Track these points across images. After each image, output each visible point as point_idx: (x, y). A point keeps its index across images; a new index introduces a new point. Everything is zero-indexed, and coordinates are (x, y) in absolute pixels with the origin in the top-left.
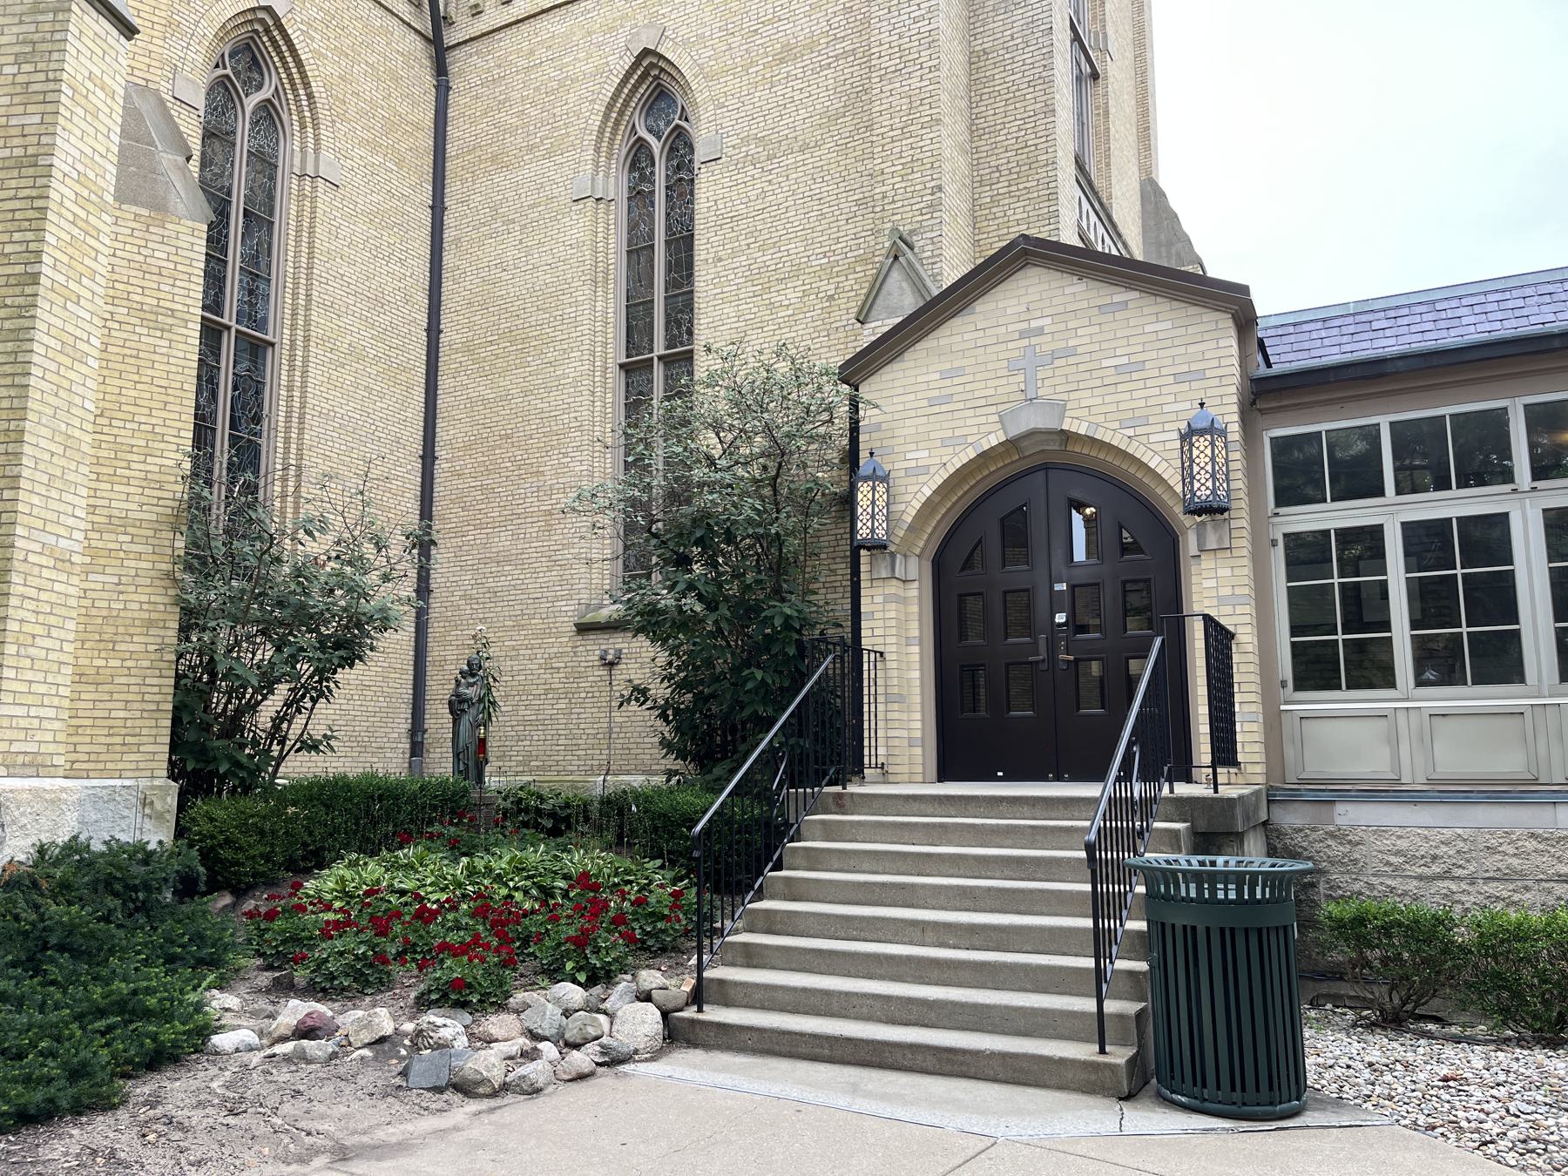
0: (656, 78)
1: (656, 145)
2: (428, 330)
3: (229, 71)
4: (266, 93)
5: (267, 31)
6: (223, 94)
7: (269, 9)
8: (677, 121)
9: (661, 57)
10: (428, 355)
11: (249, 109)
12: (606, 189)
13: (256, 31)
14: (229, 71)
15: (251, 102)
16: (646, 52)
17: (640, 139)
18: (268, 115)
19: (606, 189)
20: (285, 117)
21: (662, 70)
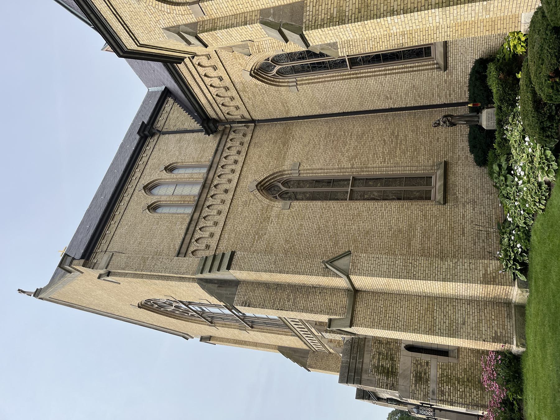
0: (257, 70)
1: (278, 68)
2: (344, 112)
3: (277, 195)
4: (280, 185)
5: (262, 186)
6: (283, 196)
7: (257, 186)
8: (270, 62)
9: (251, 70)
10: (351, 112)
11: (286, 189)
12: (297, 173)
13: (264, 188)
14: (277, 195)
15: (284, 189)
16: (251, 75)
17: (276, 73)
18: (286, 183)
19: (297, 173)
20: (285, 179)
21: (255, 69)
